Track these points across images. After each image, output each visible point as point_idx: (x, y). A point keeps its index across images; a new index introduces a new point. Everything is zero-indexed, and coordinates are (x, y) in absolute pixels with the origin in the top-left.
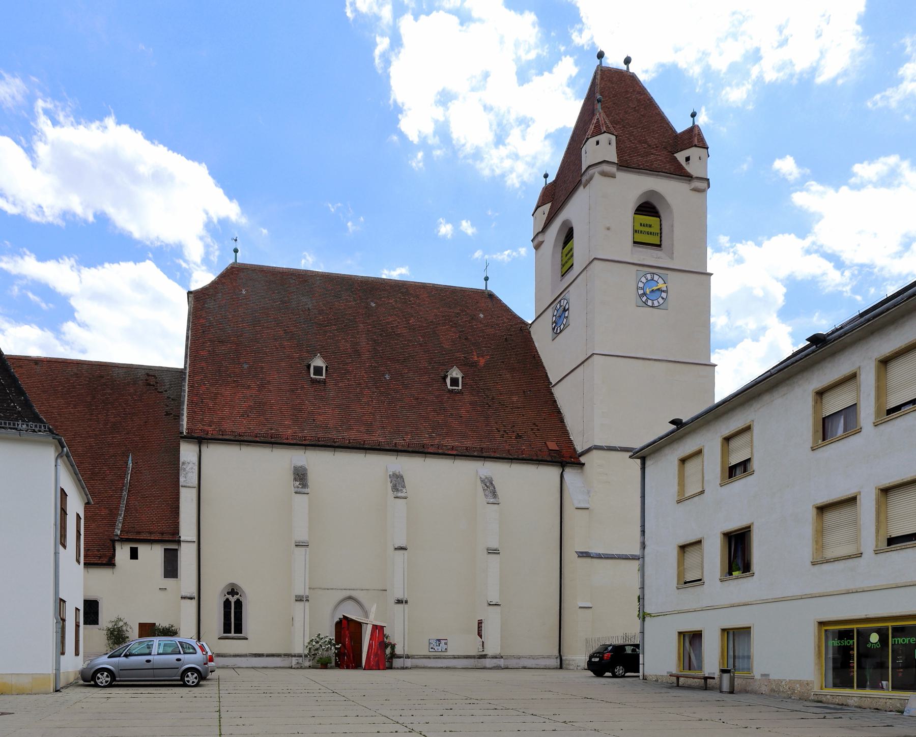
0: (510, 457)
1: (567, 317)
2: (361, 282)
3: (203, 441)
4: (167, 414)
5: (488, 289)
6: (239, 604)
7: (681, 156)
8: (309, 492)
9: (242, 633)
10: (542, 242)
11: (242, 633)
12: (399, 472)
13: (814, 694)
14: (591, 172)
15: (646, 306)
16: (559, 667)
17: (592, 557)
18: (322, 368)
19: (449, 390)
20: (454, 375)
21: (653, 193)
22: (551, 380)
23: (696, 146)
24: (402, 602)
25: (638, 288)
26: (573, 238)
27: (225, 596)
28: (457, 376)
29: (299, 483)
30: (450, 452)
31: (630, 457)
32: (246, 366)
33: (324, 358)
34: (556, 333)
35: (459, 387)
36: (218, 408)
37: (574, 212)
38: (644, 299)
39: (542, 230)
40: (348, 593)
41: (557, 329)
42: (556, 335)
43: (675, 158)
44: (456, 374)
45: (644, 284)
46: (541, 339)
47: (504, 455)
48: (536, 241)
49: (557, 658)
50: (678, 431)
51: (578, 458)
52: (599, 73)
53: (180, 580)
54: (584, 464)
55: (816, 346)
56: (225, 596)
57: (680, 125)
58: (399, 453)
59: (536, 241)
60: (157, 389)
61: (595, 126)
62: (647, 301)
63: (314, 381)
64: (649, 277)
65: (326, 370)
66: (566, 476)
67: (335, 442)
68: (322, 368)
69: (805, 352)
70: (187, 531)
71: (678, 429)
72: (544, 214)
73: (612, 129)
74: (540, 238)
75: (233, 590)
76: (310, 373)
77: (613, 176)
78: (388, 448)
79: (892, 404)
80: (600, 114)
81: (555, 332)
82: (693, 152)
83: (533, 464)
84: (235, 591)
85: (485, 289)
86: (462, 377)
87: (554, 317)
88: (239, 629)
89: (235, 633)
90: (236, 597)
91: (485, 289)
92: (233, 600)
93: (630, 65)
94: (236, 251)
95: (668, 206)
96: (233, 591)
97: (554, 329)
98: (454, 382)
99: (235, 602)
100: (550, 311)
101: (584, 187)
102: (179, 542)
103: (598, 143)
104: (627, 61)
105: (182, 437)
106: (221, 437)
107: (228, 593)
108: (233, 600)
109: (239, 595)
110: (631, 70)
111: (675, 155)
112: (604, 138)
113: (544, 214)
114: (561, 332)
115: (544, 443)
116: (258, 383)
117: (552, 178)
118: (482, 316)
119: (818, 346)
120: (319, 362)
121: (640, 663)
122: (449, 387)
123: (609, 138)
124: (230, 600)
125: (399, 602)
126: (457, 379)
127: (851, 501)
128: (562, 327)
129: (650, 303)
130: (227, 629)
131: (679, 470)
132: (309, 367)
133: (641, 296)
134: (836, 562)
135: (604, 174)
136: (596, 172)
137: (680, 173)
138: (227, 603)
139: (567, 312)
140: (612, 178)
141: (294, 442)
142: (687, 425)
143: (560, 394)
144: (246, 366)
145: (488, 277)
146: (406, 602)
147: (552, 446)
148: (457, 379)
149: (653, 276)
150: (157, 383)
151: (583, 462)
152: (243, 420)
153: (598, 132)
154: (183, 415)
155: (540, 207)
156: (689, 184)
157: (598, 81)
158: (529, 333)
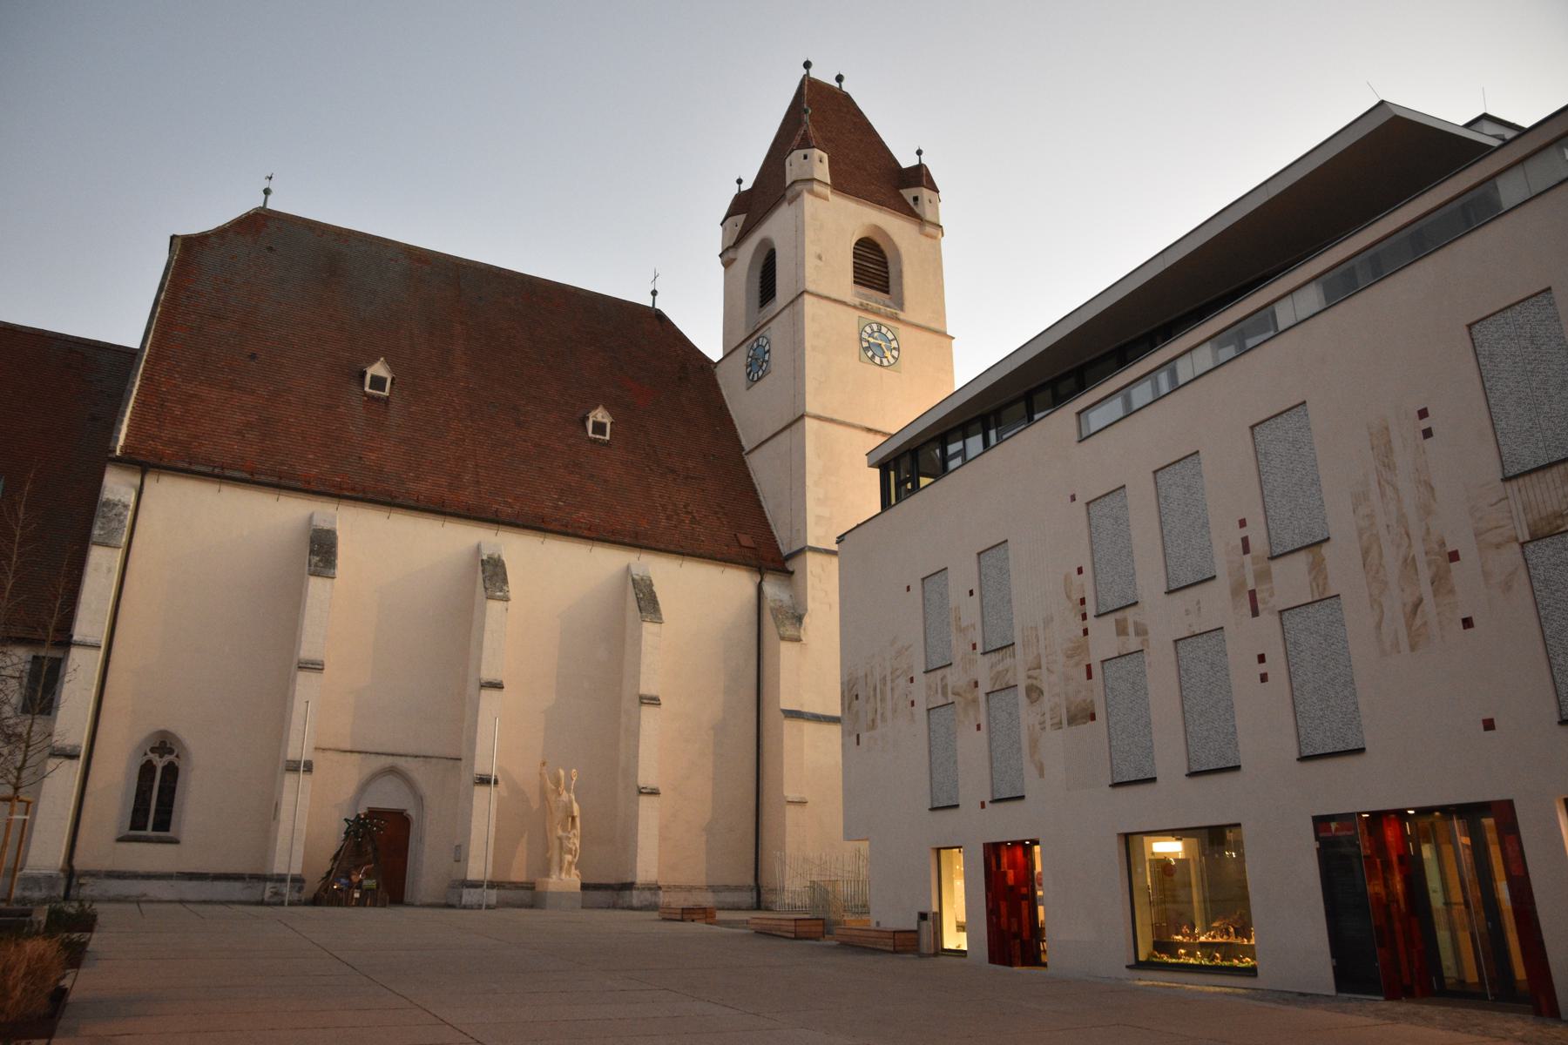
1: (767, 361)
5: (657, 307)
6: (171, 772)
9: (168, 830)
10: (734, 260)
11: (168, 830)
14: (798, 187)
16: (755, 906)
19: (590, 439)
21: (877, 228)
22: (744, 443)
26: (774, 295)
27: (146, 754)
30: (586, 533)
31: (660, 704)
33: (392, 364)
34: (752, 380)
35: (605, 435)
37: (775, 228)
39: (734, 244)
42: (752, 383)
44: (603, 417)
46: (732, 386)
48: (726, 257)
49: (752, 890)
51: (784, 564)
62: (873, 356)
63: (372, 398)
65: (392, 383)
70: (89, 622)
74: (731, 255)
75: (163, 743)
77: (826, 199)
81: (751, 378)
82: (925, 193)
84: (168, 746)
85: (651, 306)
86: (612, 423)
88: (163, 823)
90: (168, 758)
92: (160, 763)
96: (164, 744)
97: (749, 374)
98: (599, 428)
99: (164, 768)
100: (744, 349)
103: (805, 157)
104: (839, 78)
107: (153, 750)
108: (160, 763)
109: (175, 754)
114: (759, 379)
122: (590, 434)
124: (155, 763)
126: (604, 425)
128: (760, 373)
133: (866, 349)
137: (910, 212)
138: (147, 770)
141: (322, 488)
147: (746, 540)
148: (604, 425)
151: (791, 569)
153: (806, 143)
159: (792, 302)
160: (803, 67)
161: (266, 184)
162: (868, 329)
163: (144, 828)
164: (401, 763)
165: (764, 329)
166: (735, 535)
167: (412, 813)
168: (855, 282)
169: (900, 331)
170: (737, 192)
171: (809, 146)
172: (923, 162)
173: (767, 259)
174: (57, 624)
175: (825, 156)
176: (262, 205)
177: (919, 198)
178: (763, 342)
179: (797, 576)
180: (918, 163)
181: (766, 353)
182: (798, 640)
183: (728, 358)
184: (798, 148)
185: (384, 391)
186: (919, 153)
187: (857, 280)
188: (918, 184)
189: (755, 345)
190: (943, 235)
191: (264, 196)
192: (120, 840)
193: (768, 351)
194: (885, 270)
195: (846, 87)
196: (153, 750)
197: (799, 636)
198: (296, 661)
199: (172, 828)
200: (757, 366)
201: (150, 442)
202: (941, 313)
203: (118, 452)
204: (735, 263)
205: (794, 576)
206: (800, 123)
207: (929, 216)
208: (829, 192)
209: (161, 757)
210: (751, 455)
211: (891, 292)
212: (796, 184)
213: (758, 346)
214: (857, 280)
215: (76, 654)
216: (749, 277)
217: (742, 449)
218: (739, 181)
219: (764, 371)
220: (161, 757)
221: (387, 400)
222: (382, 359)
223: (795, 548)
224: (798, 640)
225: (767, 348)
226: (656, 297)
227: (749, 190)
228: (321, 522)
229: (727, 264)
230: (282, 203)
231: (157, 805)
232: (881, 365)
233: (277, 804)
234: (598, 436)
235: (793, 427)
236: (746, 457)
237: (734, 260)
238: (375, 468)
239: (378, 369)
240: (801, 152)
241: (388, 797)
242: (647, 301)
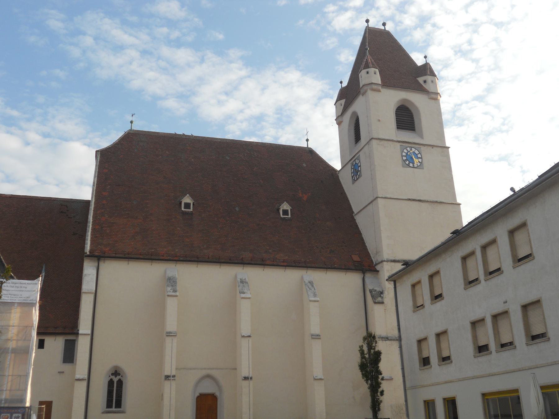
0: (325, 266)
1: (360, 171)
2: (220, 142)
3: (101, 258)
4: (75, 234)
5: (309, 147)
6: (120, 383)
7: (421, 80)
8: (178, 295)
9: (121, 408)
10: (342, 122)
11: (121, 408)
12: (245, 279)
14: (365, 88)
15: (409, 167)
17: (391, 340)
18: (190, 204)
21: (405, 100)
22: (354, 210)
23: (428, 75)
24: (248, 379)
25: (402, 156)
26: (360, 139)
27: (110, 376)
28: (287, 209)
29: (170, 288)
30: (282, 264)
32: (135, 203)
33: (192, 196)
35: (288, 215)
36: (114, 234)
37: (358, 106)
38: (407, 162)
40: (205, 372)
41: (355, 177)
43: (418, 81)
44: (287, 207)
46: (346, 181)
47: (321, 266)
50: (407, 268)
51: (374, 267)
52: (367, 30)
53: (76, 364)
54: (378, 271)
55: (456, 235)
56: (110, 376)
57: (419, 60)
58: (244, 265)
60: (67, 215)
61: (365, 63)
62: (409, 164)
63: (184, 213)
64: (409, 149)
65: (193, 205)
66: (367, 280)
67: (198, 258)
68: (190, 204)
69: (467, 227)
70: (84, 327)
71: (407, 267)
72: (341, 105)
73: (376, 65)
74: (340, 119)
75: (116, 371)
76: (181, 207)
77: (379, 91)
78: (236, 261)
79: (491, 269)
80: (369, 58)
82: (429, 78)
84: (118, 372)
85: (307, 147)
86: (291, 210)
87: (352, 170)
88: (119, 404)
89: (116, 407)
90: (118, 377)
91: (307, 147)
92: (115, 380)
93: (386, 26)
94: (132, 122)
95: (417, 109)
96: (116, 372)
97: (353, 177)
99: (117, 382)
102: (77, 334)
103: (368, 73)
105: (86, 256)
106: (114, 255)
107: (112, 374)
108: (115, 380)
109: (121, 376)
110: (387, 29)
111: (418, 79)
112: (372, 70)
113: (341, 105)
114: (357, 179)
115: (350, 256)
116: (143, 215)
117: (345, 84)
118: (304, 165)
119: (457, 234)
120: (187, 199)
122: (282, 216)
123: (374, 71)
124: (113, 380)
125: (246, 378)
126: (287, 211)
127: (483, 320)
129: (411, 165)
130: (109, 405)
131: (462, 265)
132: (181, 203)
134: (483, 356)
136: (368, 89)
137: (420, 89)
138: (111, 383)
139: (360, 167)
140: (378, 92)
141: (169, 258)
142: (463, 233)
143: (360, 220)
144: (135, 203)
145: (308, 139)
146: (251, 378)
147: (356, 258)
148: (287, 211)
149: (412, 149)
150: (68, 211)
152: (131, 242)
153: (367, 66)
154: (87, 240)
155: (338, 101)
157: (367, 35)
158: (338, 177)
159: (368, 142)
161: (131, 119)
162: (405, 151)
163: (111, 407)
164: (213, 373)
165: (358, 155)
166: (351, 256)
167: (217, 394)
168: (397, 128)
169: (422, 149)
171: (368, 67)
172: (428, 62)
173: (355, 124)
175: (377, 71)
176: (130, 129)
178: (357, 161)
179: (381, 273)
181: (359, 167)
182: (383, 303)
183: (344, 169)
184: (364, 69)
185: (190, 209)
187: (398, 127)
188: (425, 74)
189: (354, 163)
190: (441, 97)
192: (103, 413)
193: (360, 166)
196: (112, 374)
197: (383, 301)
198: (165, 333)
199: (122, 406)
200: (356, 173)
201: (99, 246)
203: (88, 253)
206: (365, 54)
207: (431, 89)
209: (116, 377)
212: (365, 86)
213: (355, 163)
214: (398, 127)
215: (80, 337)
216: (349, 130)
217: (353, 212)
218: (341, 82)
219: (359, 176)
220: (116, 377)
221: (191, 213)
222: (188, 195)
223: (380, 260)
224: (383, 303)
227: (346, 86)
228: (170, 274)
229: (339, 123)
230: (141, 125)
231: (116, 396)
232: (413, 167)
233: (162, 394)
234: (285, 216)
235: (373, 203)
236: (355, 216)
238: (190, 245)
239: (187, 199)
241: (208, 388)
242: (305, 145)
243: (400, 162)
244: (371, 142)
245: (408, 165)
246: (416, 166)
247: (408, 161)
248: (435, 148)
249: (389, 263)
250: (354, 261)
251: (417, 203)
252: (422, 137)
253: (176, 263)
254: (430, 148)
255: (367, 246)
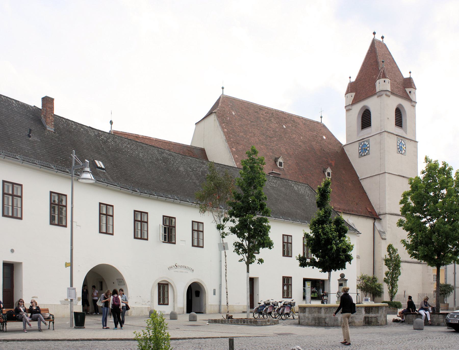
10: (351, 109)
13: (226, 322)
20: (329, 171)
21: (400, 105)
25: (397, 145)
42: (361, 156)
43: (406, 91)
44: (329, 171)
45: (399, 144)
51: (378, 216)
54: (381, 219)
59: (348, 108)
66: (376, 223)
68: (282, 163)
74: (350, 107)
77: (389, 96)
81: (361, 154)
83: (365, 218)
86: (332, 172)
101: (378, 97)
103: (384, 81)
110: (384, 42)
117: (353, 80)
121: (166, 297)
122: (278, 166)
128: (365, 154)
135: (387, 95)
140: (388, 97)
151: (381, 218)
156: (411, 103)
160: (373, 34)
168: (396, 125)
170: (349, 82)
174: (264, 219)
177: (411, 92)
180: (409, 77)
186: (410, 73)
189: (363, 143)
191: (321, 118)
194: (401, 119)
195: (385, 41)
202: (414, 134)
204: (352, 110)
205: (381, 220)
207: (413, 100)
208: (390, 94)
210: (362, 180)
211: (403, 127)
213: (364, 144)
218: (350, 78)
225: (368, 146)
226: (224, 90)
227: (354, 82)
232: (402, 154)
237: (350, 109)
240: (384, 79)
243: (396, 149)
244: (383, 133)
245: (399, 152)
246: (403, 153)
247: (400, 149)
248: (412, 142)
249: (389, 215)
250: (369, 212)
251: (402, 178)
252: (406, 132)
253: (351, 216)
254: (410, 141)
255: (371, 202)
